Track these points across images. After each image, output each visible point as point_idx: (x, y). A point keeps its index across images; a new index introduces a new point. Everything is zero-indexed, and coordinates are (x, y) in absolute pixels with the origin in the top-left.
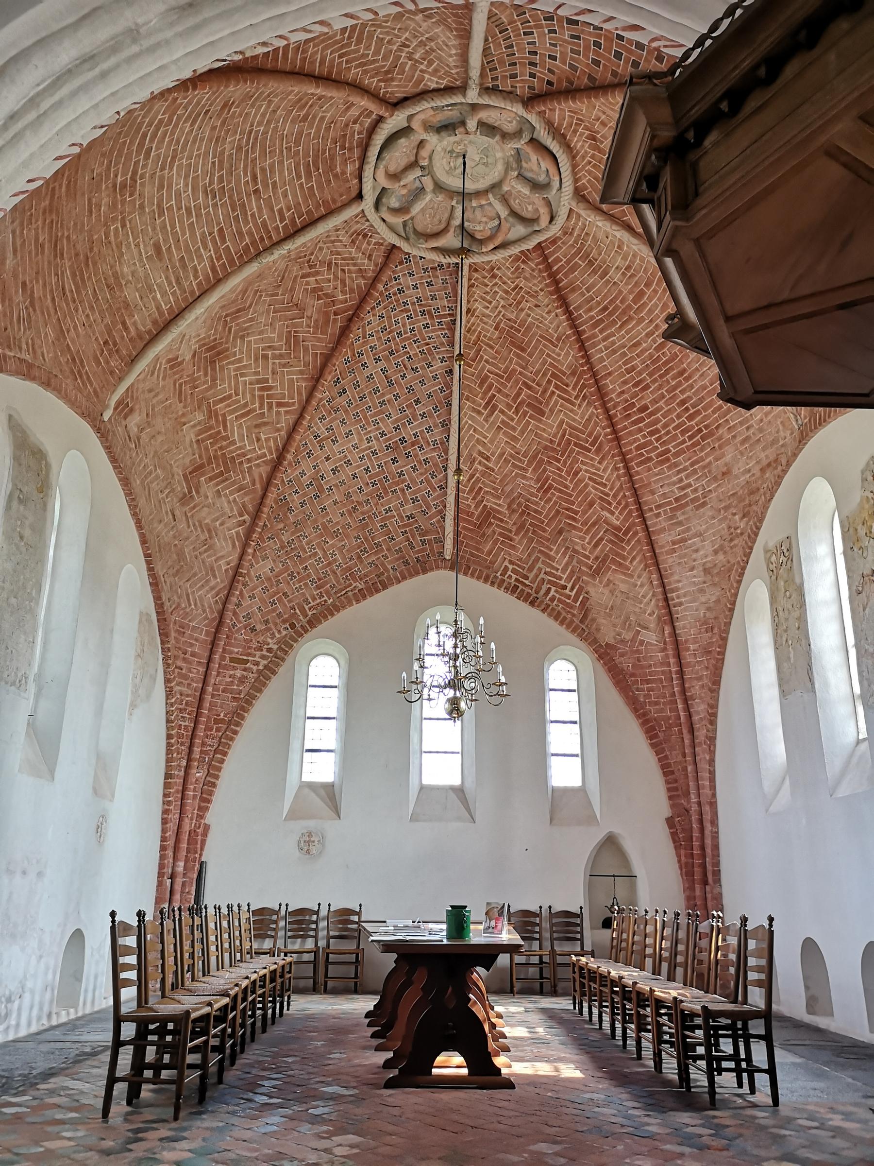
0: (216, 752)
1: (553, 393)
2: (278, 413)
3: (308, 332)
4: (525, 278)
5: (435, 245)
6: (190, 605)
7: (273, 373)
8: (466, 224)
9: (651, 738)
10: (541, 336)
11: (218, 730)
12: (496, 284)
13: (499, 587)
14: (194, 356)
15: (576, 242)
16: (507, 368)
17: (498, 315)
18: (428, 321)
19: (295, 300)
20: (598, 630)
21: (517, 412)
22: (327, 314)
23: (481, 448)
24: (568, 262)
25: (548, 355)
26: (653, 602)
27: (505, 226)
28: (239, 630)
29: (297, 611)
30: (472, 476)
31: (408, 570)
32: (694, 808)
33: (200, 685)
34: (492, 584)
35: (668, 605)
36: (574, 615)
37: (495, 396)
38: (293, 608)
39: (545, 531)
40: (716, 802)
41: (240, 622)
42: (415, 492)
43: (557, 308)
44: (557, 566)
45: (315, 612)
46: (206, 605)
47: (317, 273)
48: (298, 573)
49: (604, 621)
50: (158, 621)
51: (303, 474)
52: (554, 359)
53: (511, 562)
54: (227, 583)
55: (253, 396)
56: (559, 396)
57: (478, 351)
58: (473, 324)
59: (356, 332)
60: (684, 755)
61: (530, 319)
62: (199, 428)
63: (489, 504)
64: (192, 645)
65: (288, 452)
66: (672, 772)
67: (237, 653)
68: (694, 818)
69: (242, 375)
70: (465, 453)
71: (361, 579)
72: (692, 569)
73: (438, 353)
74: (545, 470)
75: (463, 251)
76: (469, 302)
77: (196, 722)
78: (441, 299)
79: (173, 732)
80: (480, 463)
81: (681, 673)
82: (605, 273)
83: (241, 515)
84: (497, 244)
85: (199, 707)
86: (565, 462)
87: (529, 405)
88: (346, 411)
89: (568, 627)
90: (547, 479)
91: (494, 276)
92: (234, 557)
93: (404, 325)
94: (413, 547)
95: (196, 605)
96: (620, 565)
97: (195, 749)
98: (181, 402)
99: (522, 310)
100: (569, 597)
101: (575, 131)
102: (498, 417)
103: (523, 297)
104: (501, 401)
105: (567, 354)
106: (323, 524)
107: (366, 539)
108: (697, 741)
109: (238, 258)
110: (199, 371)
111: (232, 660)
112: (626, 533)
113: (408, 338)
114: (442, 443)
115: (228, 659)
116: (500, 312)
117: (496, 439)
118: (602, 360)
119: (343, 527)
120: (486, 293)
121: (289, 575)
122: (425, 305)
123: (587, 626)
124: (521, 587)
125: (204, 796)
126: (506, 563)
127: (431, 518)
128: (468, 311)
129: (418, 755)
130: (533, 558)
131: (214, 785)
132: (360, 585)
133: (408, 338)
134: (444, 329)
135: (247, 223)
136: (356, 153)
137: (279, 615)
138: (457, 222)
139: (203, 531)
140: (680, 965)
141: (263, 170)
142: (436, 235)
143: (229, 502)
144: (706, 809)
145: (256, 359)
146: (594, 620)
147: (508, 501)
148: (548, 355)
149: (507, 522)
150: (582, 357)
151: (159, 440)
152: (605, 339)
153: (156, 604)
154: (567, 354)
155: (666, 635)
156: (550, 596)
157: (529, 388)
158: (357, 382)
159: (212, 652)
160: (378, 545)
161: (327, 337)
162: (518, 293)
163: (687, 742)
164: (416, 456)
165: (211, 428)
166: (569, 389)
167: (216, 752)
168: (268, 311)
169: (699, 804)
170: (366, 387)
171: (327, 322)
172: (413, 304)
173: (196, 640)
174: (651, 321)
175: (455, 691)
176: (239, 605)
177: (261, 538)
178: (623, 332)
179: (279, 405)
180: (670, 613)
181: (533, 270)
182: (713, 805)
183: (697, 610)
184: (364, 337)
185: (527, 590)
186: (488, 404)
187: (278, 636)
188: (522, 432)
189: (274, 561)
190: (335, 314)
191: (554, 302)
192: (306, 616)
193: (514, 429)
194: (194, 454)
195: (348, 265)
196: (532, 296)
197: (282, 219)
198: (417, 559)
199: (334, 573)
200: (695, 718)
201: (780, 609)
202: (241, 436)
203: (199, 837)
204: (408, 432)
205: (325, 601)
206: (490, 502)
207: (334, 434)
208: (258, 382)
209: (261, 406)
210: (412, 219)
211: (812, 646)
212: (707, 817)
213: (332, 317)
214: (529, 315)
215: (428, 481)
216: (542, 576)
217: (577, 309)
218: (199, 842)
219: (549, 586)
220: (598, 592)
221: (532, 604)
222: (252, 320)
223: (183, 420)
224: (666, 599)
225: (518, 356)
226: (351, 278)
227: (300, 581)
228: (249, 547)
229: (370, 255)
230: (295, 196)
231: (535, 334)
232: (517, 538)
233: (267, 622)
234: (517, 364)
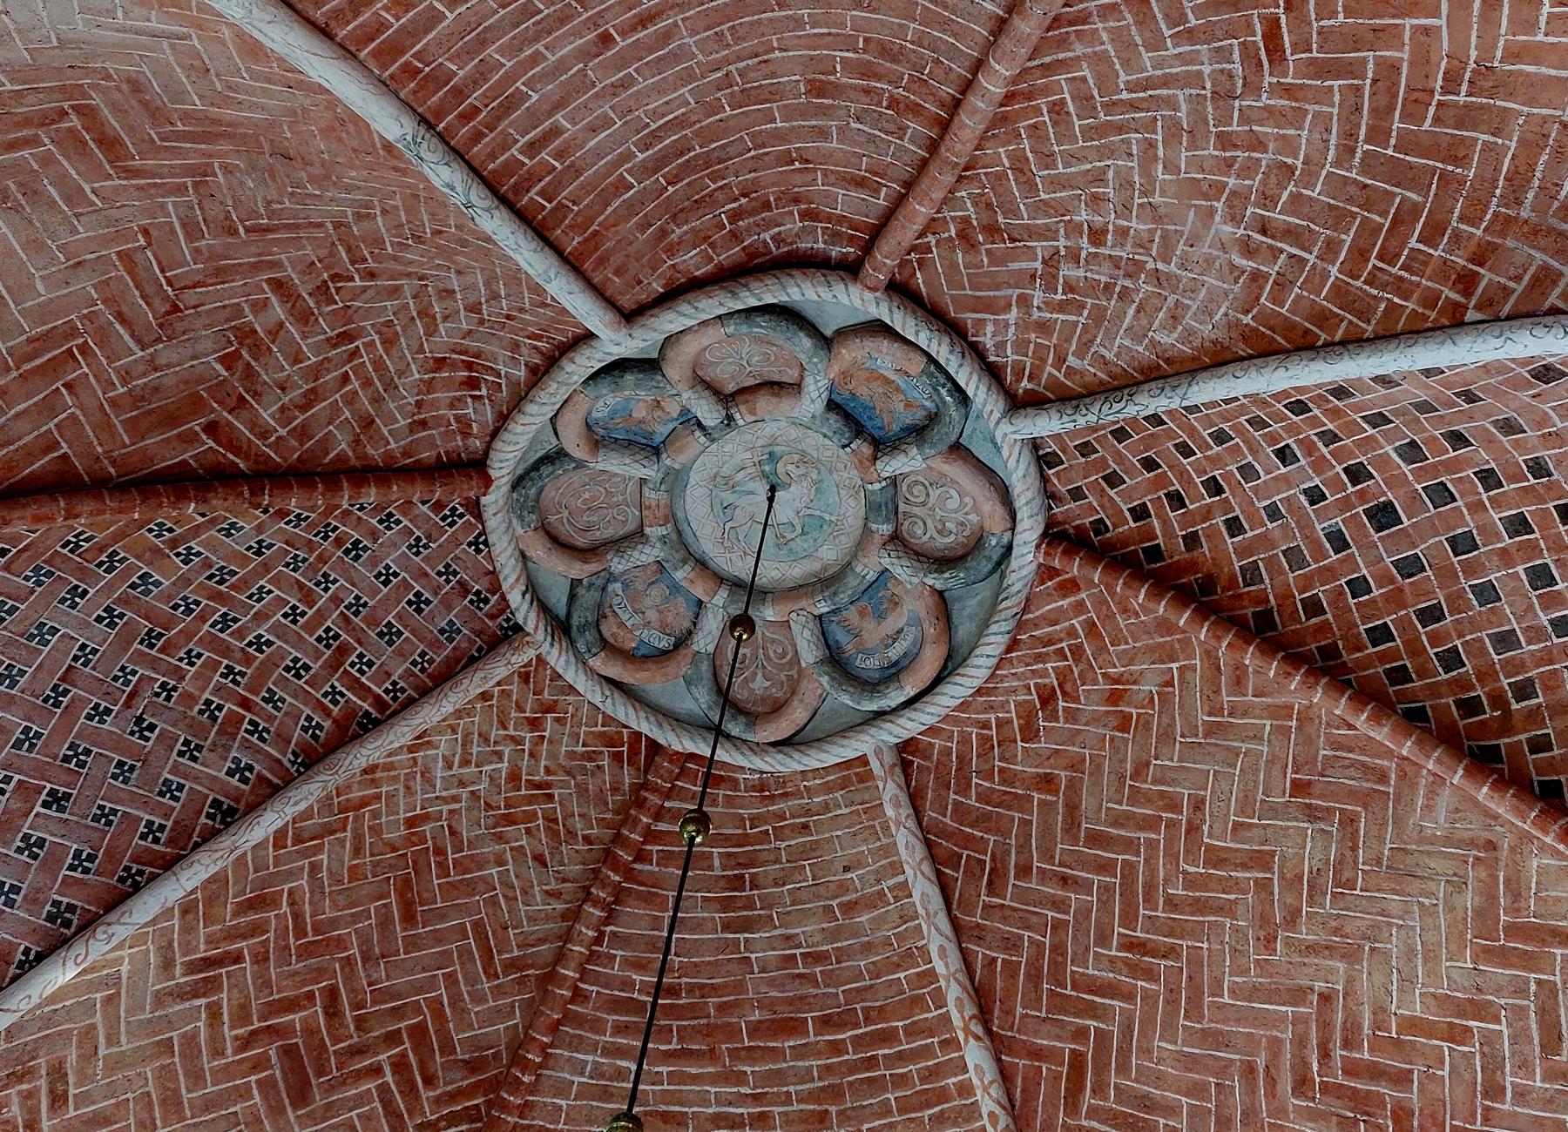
1: (377, 1070)
4: (582, 790)
10: (478, 927)
12: (517, 741)
15: (755, 820)
16: (334, 923)
17: (445, 800)
18: (315, 667)
19: (190, 297)
21: (245, 1043)
23: (72, 1057)
25: (451, 979)
27: (681, 666)
37: (238, 958)
47: (305, 318)
52: (456, 1000)
78: (401, 654)
82: (746, 926)
87: (289, 1052)
91: (534, 724)
93: (260, 617)
99: (500, 838)
101: (1040, 658)
102: (193, 1015)
103: (532, 816)
104: (238, 985)
109: (407, 64)
113: (225, 651)
116: (456, 799)
117: (131, 1065)
118: (562, 1089)
134: (327, 712)
135: (513, 49)
136: (730, 255)
141: (667, 36)
142: (558, 543)
148: (451, 979)
157: (332, 1012)
162: (531, 800)
166: (426, 1094)
168: (121, 236)
171: (170, 418)
172: (336, 600)
174: (757, 1098)
184: (173, 544)
186: (209, 963)
188: (208, 1105)
190: (212, 429)
193: (196, 1078)
195: (367, 383)
196: (553, 834)
197: (532, 148)
213: (196, 425)
214: (500, 862)
222: (74, 196)
225: (385, 922)
226: (335, 410)
229: (423, 424)
230: (598, 154)
234: (365, 940)
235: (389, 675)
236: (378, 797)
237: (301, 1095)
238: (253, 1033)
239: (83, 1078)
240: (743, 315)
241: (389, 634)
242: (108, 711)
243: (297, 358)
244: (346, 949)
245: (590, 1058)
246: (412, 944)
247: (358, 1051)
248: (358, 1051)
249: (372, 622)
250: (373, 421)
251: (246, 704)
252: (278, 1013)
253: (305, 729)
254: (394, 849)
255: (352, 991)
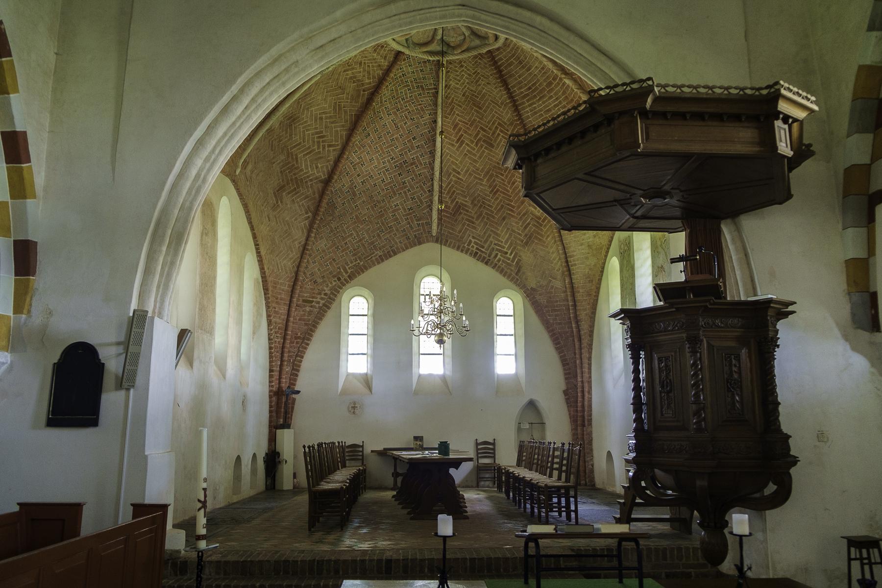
0: (297, 356)
1: (499, 134)
2: (329, 151)
3: (347, 102)
4: (482, 68)
5: (426, 50)
6: (279, 270)
7: (326, 128)
8: (444, 38)
9: (556, 344)
11: (297, 343)
12: (463, 70)
13: (466, 253)
14: (280, 124)
15: (511, 50)
18: (421, 92)
20: (526, 279)
21: (477, 145)
22: (359, 91)
24: (507, 60)
26: (559, 262)
27: (468, 40)
28: (307, 283)
29: (342, 270)
30: (449, 183)
31: (410, 243)
32: (580, 384)
33: (286, 317)
34: (462, 251)
35: (568, 265)
36: (512, 270)
37: (462, 135)
38: (339, 268)
39: (494, 217)
40: (591, 381)
41: (307, 278)
42: (413, 194)
43: (500, 87)
44: (502, 240)
45: (352, 270)
46: (288, 269)
47: (353, 69)
48: (342, 247)
49: (530, 274)
50: (262, 281)
51: (344, 185)
52: (499, 115)
53: (473, 237)
54: (299, 255)
55: (314, 142)
56: (502, 136)
57: (452, 109)
58: (449, 93)
59: (377, 99)
60: (575, 354)
61: (484, 91)
62: (282, 164)
63: (460, 201)
64: (280, 294)
65: (335, 174)
66: (568, 364)
67: (307, 297)
68: (579, 390)
69: (308, 130)
70: (445, 170)
71: (380, 249)
72: (582, 244)
73: (427, 110)
74: (494, 181)
75: (443, 53)
76: (446, 81)
77: (285, 339)
78: (429, 79)
79: (273, 346)
80: (454, 176)
81: (575, 305)
82: (529, 69)
83: (307, 213)
84: (463, 49)
85: (286, 330)
86: (507, 176)
87: (484, 141)
88: (370, 147)
89: (508, 278)
90: (496, 186)
92: (303, 239)
94: (412, 228)
95: (282, 269)
96: (540, 240)
97: (285, 355)
98: (272, 151)
99: (479, 85)
100: (509, 259)
102: (465, 148)
105: (507, 112)
106: (356, 216)
107: (383, 224)
108: (582, 346)
110: (282, 131)
111: (304, 301)
112: (543, 221)
113: (409, 101)
114: (430, 164)
115: (301, 300)
116: (466, 86)
118: (528, 117)
119: (368, 217)
120: (458, 76)
121: (336, 248)
122: (419, 83)
123: (520, 277)
124: (479, 253)
125: (292, 381)
126: (471, 238)
127: (423, 210)
128: (446, 86)
129: (418, 357)
130: (487, 235)
131: (297, 375)
132: (380, 253)
133: (409, 101)
137: (331, 273)
138: (439, 37)
139: (285, 225)
140: (556, 469)
142: (426, 44)
143: (300, 206)
144: (586, 385)
145: (316, 120)
146: (524, 273)
147: (472, 198)
148: (495, 112)
149: (471, 212)
150: (517, 116)
151: (261, 175)
152: (530, 105)
153: (261, 272)
154: (507, 112)
155: (566, 283)
156: (497, 259)
157: (484, 130)
158: (377, 129)
159: (292, 297)
160: (390, 227)
161: (359, 104)
162: (476, 76)
163: (577, 346)
164: (414, 171)
165: (289, 163)
167: (297, 356)
169: (582, 382)
170: (382, 131)
171: (358, 96)
173: (283, 290)
174: (557, 98)
175: (441, 330)
176: (307, 267)
177: (319, 227)
178: (541, 103)
179: (330, 146)
180: (569, 270)
181: (486, 64)
182: (590, 382)
183: (584, 269)
184: (381, 102)
185: (483, 255)
186: (458, 140)
187: (330, 285)
189: (327, 240)
190: (364, 91)
191: (499, 83)
192: (347, 272)
193: (475, 155)
194: (279, 180)
195: (372, 63)
198: (415, 235)
199: (363, 245)
200: (582, 332)
201: (624, 276)
202: (306, 166)
203: (290, 405)
204: (410, 156)
205: (359, 263)
206: (460, 199)
207: (362, 161)
208: (317, 133)
209: (319, 148)
210: (411, 37)
211: (637, 300)
212: (586, 389)
213: (362, 93)
215: (421, 187)
216: (493, 245)
217: (514, 86)
218: (290, 408)
219: (497, 252)
220: (527, 256)
221: (486, 263)
222: (313, 98)
223: (274, 161)
224: (567, 262)
227: (343, 251)
228: (312, 232)
229: (386, 57)
231: (487, 100)
232: (477, 222)
233: (323, 277)
234: (478, 117)
235: (431, 83)
236: (453, 98)
237: (492, 146)
238: (476, 142)
239: (459, 168)
240: (369, 82)
241: (424, 78)
242: (406, 122)
243: (360, 72)
244: (476, 120)
245: (527, 109)
246: (485, 111)
247: (494, 133)
248: (494, 133)
249: (420, 79)
250: (379, 65)
251: (420, 105)
252: (477, 136)
253: (431, 101)
254: (466, 101)
255: (484, 125)
